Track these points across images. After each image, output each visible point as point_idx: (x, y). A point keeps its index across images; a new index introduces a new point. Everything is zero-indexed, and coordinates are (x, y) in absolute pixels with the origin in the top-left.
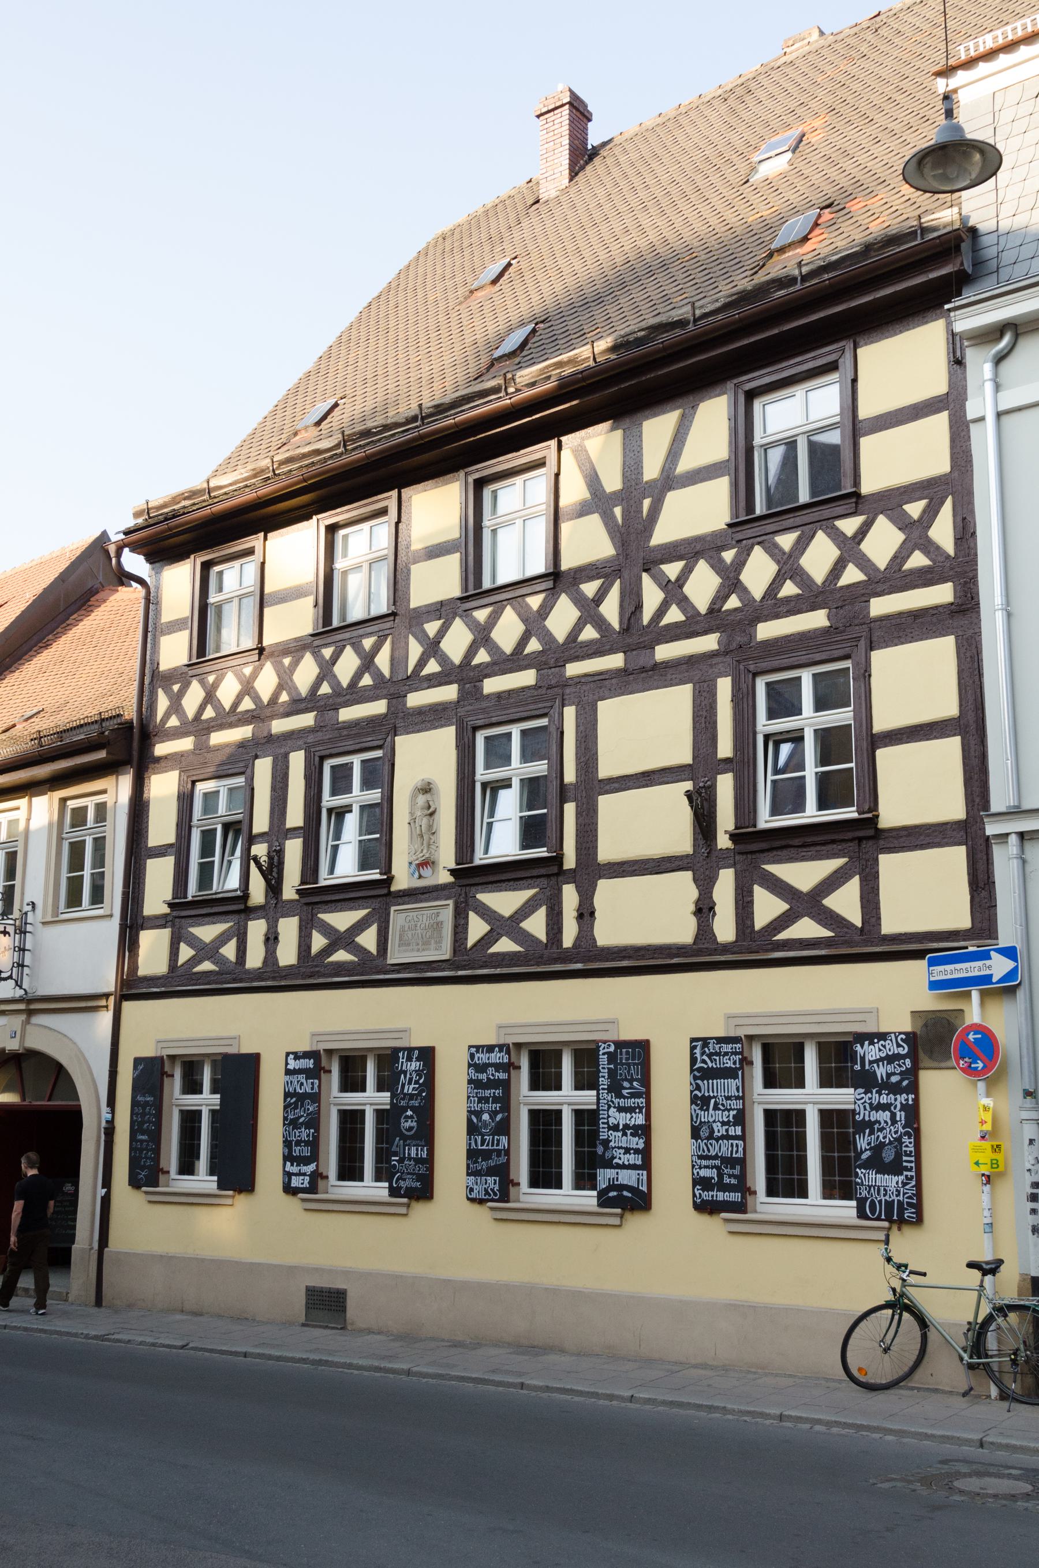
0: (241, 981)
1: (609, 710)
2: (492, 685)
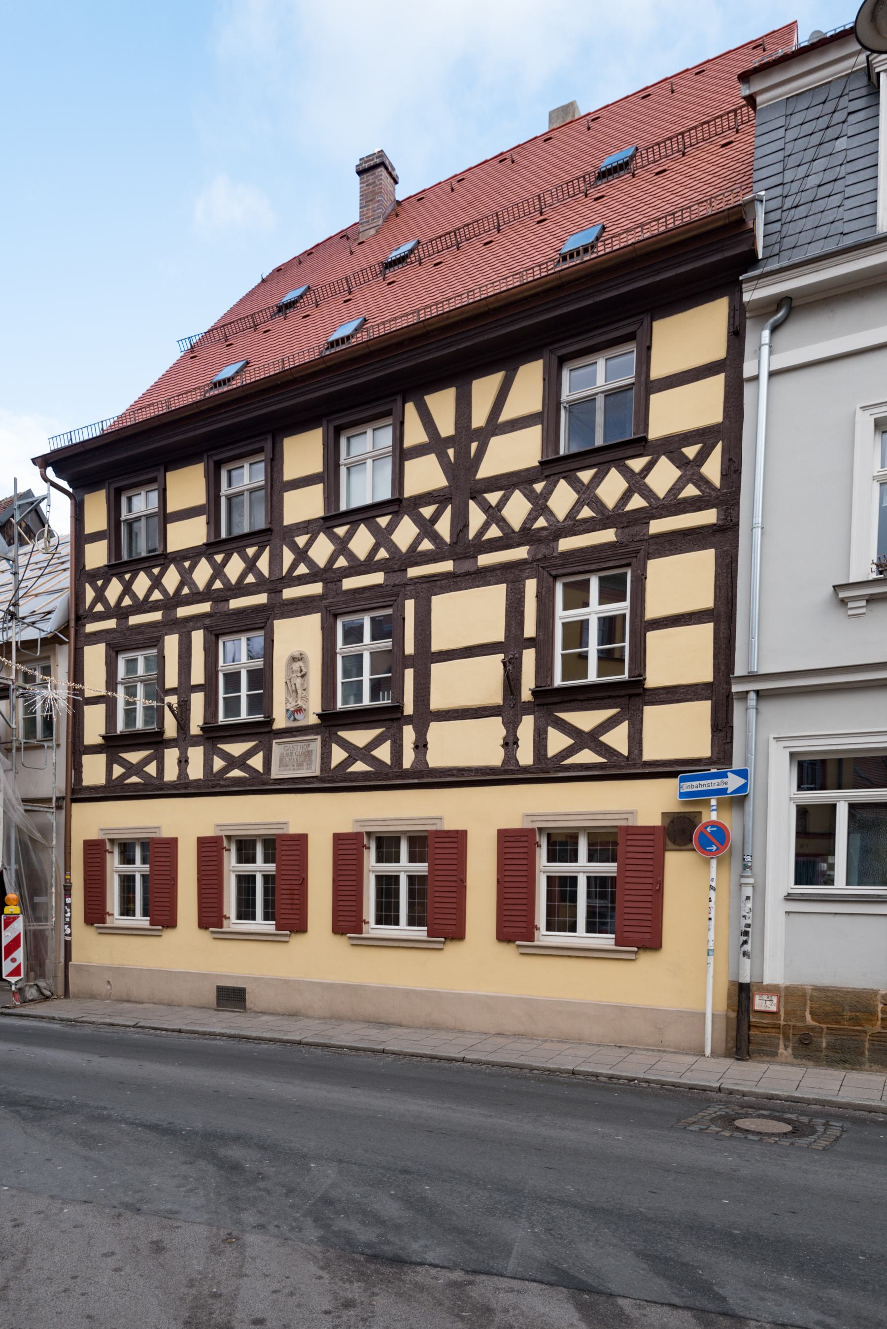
0: (161, 789)
1: (439, 602)
2: (348, 584)
